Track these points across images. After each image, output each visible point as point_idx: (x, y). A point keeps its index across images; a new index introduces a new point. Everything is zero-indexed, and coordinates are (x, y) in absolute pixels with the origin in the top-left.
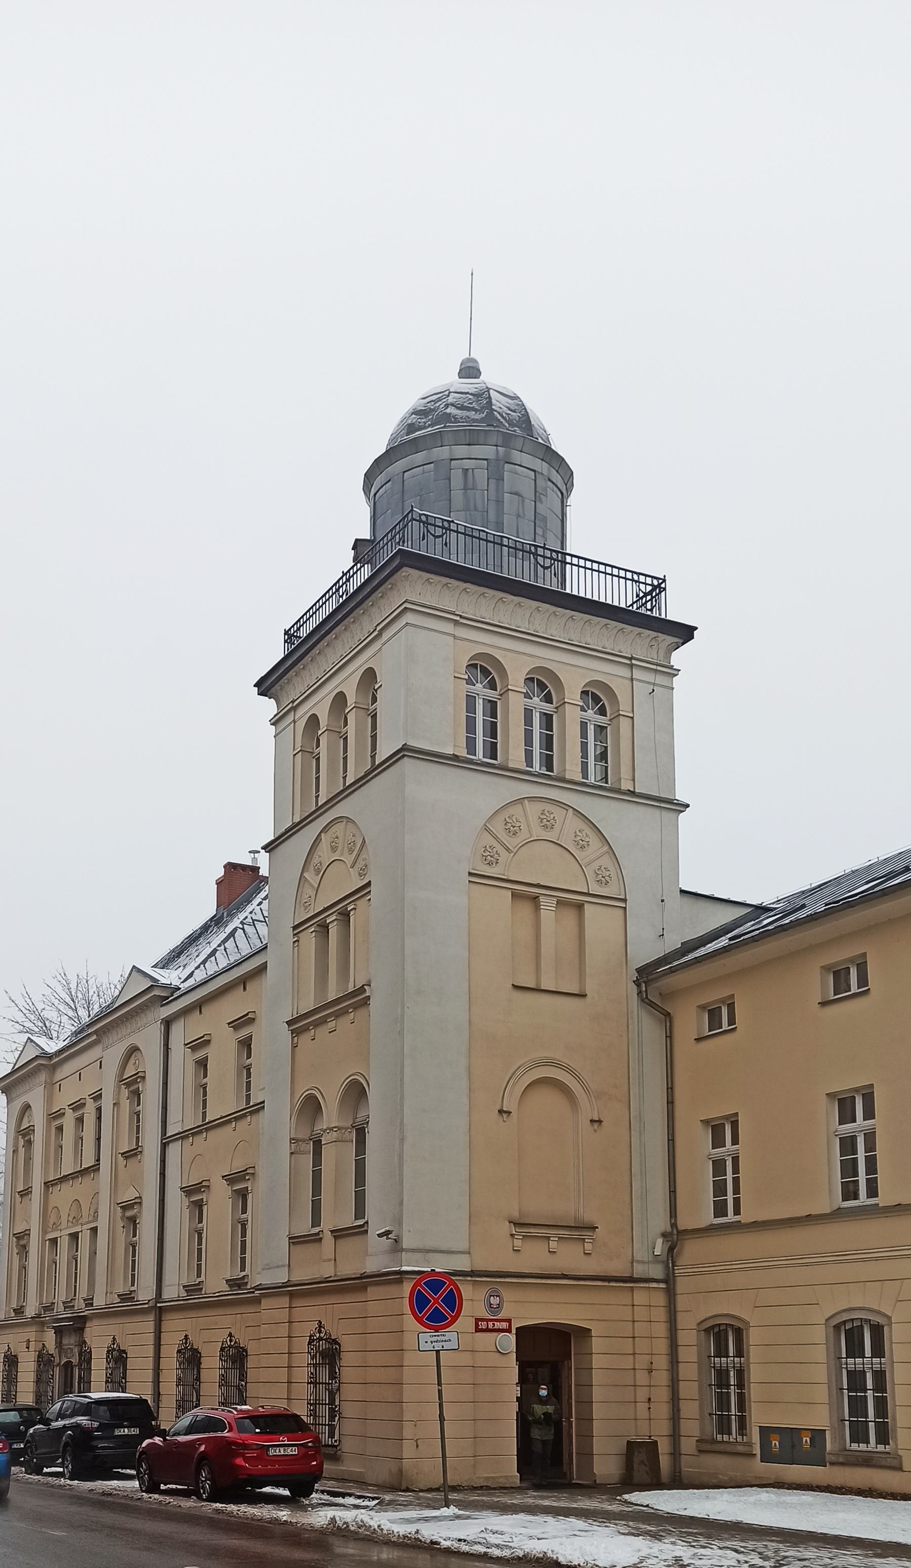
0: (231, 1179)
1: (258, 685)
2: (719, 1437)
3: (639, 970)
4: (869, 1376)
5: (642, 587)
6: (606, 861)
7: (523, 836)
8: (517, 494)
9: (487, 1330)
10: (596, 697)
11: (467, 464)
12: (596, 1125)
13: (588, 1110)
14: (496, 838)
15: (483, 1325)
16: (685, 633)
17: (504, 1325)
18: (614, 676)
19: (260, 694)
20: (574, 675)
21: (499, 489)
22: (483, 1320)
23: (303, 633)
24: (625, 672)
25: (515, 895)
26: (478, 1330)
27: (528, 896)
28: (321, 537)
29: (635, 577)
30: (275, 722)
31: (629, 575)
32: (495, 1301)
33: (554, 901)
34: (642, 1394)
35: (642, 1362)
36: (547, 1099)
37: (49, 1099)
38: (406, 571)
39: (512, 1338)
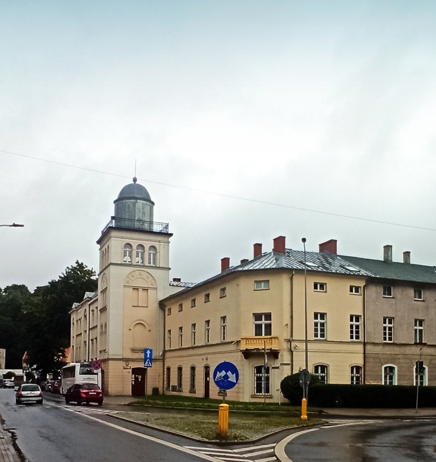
0: (95, 338)
1: (97, 242)
2: (266, 394)
3: (160, 302)
4: (263, 378)
5: (163, 226)
6: (153, 281)
7: (135, 277)
8: (139, 209)
9: (126, 369)
10: (153, 247)
11: (129, 203)
12: (149, 331)
13: (148, 328)
14: (130, 279)
15: (125, 368)
16: (171, 235)
17: (129, 368)
18: (156, 244)
19: (97, 244)
20: (147, 245)
21: (135, 208)
22: (125, 367)
23: (104, 231)
24: (158, 243)
25: (133, 289)
26: (124, 369)
27: (136, 289)
28: (106, 215)
29: (162, 224)
30: (100, 250)
31: (160, 224)
32: (127, 364)
33: (142, 289)
34: (157, 380)
35: (158, 374)
36: (140, 327)
37: (77, 317)
38: (111, 230)
39: (131, 370)
